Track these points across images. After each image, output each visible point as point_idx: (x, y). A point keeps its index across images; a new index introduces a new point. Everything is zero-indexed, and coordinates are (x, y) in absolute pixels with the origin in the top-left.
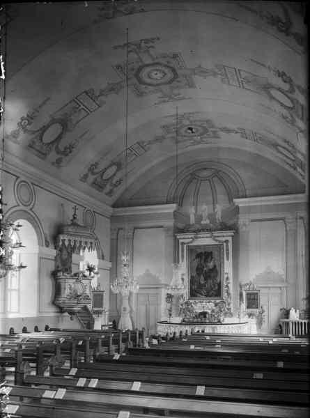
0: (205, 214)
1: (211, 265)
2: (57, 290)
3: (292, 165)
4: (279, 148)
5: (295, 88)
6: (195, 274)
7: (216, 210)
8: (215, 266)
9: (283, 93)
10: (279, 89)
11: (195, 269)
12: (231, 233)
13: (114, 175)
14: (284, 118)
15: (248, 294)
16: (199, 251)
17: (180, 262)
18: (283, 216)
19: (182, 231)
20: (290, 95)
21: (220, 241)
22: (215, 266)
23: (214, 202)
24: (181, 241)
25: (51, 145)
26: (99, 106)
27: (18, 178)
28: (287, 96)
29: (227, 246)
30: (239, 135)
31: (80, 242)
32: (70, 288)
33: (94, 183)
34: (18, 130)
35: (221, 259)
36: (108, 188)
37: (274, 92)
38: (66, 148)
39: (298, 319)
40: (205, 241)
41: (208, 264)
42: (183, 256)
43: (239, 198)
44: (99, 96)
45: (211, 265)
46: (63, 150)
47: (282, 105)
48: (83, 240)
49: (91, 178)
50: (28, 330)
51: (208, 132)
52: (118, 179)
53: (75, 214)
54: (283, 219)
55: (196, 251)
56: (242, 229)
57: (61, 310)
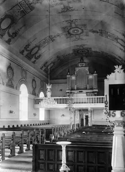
25: (5, 31)
37: (119, 40)
46: (37, 57)
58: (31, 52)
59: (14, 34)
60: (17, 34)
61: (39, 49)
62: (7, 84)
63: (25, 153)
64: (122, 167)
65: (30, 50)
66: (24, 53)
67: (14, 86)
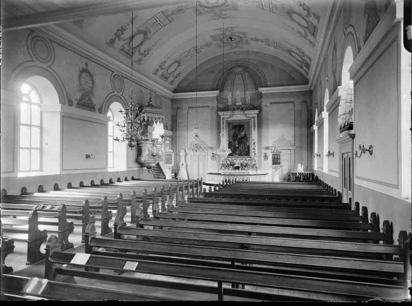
0: (239, 98)
1: (243, 134)
2: (139, 152)
3: (300, 65)
4: (292, 53)
5: (312, 15)
6: (231, 140)
7: (246, 95)
8: (246, 135)
9: (302, 17)
10: (299, 14)
11: (232, 135)
12: (257, 112)
13: (176, 69)
14: (299, 33)
15: (273, 155)
16: (235, 124)
17: (222, 132)
18: (292, 100)
19: (223, 110)
20: (307, 19)
21: (249, 117)
22: (246, 135)
23: (245, 90)
24: (222, 117)
26: (170, 22)
27: (113, 72)
28: (304, 19)
29: (254, 120)
30: (264, 43)
31: (152, 118)
32: (149, 151)
33: (162, 75)
34: (115, 38)
35: (249, 130)
36: (171, 79)
37: (295, 17)
38: (145, 51)
39: (303, 171)
40: (239, 116)
41: (241, 133)
42: (223, 128)
43: (262, 87)
45: (243, 134)
46: (142, 52)
47: (299, 24)
48: (154, 116)
49: (160, 72)
50: (121, 180)
51: (242, 40)
52: (178, 73)
53: (151, 98)
54: (293, 102)
55: (232, 124)
56: (264, 109)
57: (141, 165)
60: (124, 30)
61: (146, 38)
62: (80, 103)
66: (115, 45)
67: (96, 108)
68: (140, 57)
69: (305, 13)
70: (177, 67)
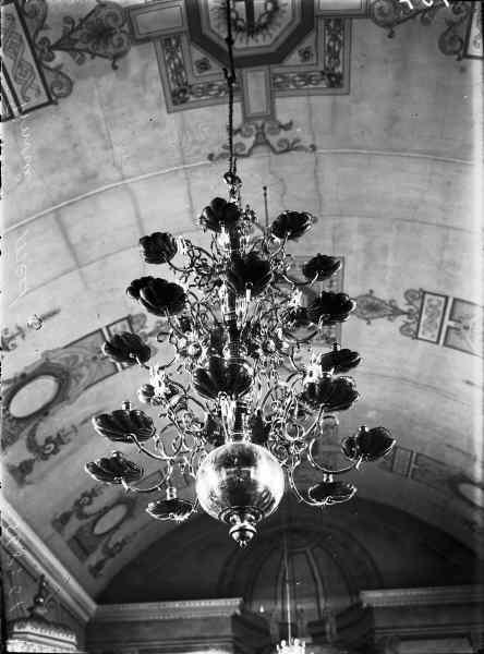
25: (22, 425)
38: (48, 441)
44: (404, 313)
46: (41, 442)
49: (74, 524)
52: (120, 540)
58: (95, 523)
59: (53, 442)
61: (61, 396)
63: (81, 353)
64: (182, 190)
65: (93, 512)
68: (28, 456)
69: (45, 430)
70: (121, 522)
